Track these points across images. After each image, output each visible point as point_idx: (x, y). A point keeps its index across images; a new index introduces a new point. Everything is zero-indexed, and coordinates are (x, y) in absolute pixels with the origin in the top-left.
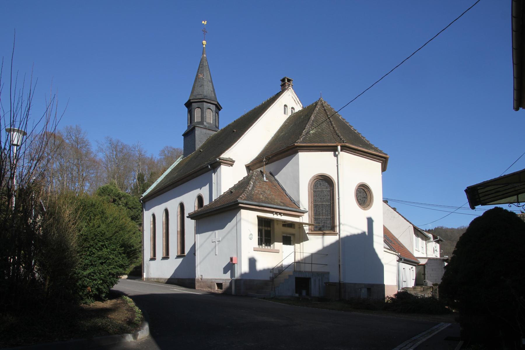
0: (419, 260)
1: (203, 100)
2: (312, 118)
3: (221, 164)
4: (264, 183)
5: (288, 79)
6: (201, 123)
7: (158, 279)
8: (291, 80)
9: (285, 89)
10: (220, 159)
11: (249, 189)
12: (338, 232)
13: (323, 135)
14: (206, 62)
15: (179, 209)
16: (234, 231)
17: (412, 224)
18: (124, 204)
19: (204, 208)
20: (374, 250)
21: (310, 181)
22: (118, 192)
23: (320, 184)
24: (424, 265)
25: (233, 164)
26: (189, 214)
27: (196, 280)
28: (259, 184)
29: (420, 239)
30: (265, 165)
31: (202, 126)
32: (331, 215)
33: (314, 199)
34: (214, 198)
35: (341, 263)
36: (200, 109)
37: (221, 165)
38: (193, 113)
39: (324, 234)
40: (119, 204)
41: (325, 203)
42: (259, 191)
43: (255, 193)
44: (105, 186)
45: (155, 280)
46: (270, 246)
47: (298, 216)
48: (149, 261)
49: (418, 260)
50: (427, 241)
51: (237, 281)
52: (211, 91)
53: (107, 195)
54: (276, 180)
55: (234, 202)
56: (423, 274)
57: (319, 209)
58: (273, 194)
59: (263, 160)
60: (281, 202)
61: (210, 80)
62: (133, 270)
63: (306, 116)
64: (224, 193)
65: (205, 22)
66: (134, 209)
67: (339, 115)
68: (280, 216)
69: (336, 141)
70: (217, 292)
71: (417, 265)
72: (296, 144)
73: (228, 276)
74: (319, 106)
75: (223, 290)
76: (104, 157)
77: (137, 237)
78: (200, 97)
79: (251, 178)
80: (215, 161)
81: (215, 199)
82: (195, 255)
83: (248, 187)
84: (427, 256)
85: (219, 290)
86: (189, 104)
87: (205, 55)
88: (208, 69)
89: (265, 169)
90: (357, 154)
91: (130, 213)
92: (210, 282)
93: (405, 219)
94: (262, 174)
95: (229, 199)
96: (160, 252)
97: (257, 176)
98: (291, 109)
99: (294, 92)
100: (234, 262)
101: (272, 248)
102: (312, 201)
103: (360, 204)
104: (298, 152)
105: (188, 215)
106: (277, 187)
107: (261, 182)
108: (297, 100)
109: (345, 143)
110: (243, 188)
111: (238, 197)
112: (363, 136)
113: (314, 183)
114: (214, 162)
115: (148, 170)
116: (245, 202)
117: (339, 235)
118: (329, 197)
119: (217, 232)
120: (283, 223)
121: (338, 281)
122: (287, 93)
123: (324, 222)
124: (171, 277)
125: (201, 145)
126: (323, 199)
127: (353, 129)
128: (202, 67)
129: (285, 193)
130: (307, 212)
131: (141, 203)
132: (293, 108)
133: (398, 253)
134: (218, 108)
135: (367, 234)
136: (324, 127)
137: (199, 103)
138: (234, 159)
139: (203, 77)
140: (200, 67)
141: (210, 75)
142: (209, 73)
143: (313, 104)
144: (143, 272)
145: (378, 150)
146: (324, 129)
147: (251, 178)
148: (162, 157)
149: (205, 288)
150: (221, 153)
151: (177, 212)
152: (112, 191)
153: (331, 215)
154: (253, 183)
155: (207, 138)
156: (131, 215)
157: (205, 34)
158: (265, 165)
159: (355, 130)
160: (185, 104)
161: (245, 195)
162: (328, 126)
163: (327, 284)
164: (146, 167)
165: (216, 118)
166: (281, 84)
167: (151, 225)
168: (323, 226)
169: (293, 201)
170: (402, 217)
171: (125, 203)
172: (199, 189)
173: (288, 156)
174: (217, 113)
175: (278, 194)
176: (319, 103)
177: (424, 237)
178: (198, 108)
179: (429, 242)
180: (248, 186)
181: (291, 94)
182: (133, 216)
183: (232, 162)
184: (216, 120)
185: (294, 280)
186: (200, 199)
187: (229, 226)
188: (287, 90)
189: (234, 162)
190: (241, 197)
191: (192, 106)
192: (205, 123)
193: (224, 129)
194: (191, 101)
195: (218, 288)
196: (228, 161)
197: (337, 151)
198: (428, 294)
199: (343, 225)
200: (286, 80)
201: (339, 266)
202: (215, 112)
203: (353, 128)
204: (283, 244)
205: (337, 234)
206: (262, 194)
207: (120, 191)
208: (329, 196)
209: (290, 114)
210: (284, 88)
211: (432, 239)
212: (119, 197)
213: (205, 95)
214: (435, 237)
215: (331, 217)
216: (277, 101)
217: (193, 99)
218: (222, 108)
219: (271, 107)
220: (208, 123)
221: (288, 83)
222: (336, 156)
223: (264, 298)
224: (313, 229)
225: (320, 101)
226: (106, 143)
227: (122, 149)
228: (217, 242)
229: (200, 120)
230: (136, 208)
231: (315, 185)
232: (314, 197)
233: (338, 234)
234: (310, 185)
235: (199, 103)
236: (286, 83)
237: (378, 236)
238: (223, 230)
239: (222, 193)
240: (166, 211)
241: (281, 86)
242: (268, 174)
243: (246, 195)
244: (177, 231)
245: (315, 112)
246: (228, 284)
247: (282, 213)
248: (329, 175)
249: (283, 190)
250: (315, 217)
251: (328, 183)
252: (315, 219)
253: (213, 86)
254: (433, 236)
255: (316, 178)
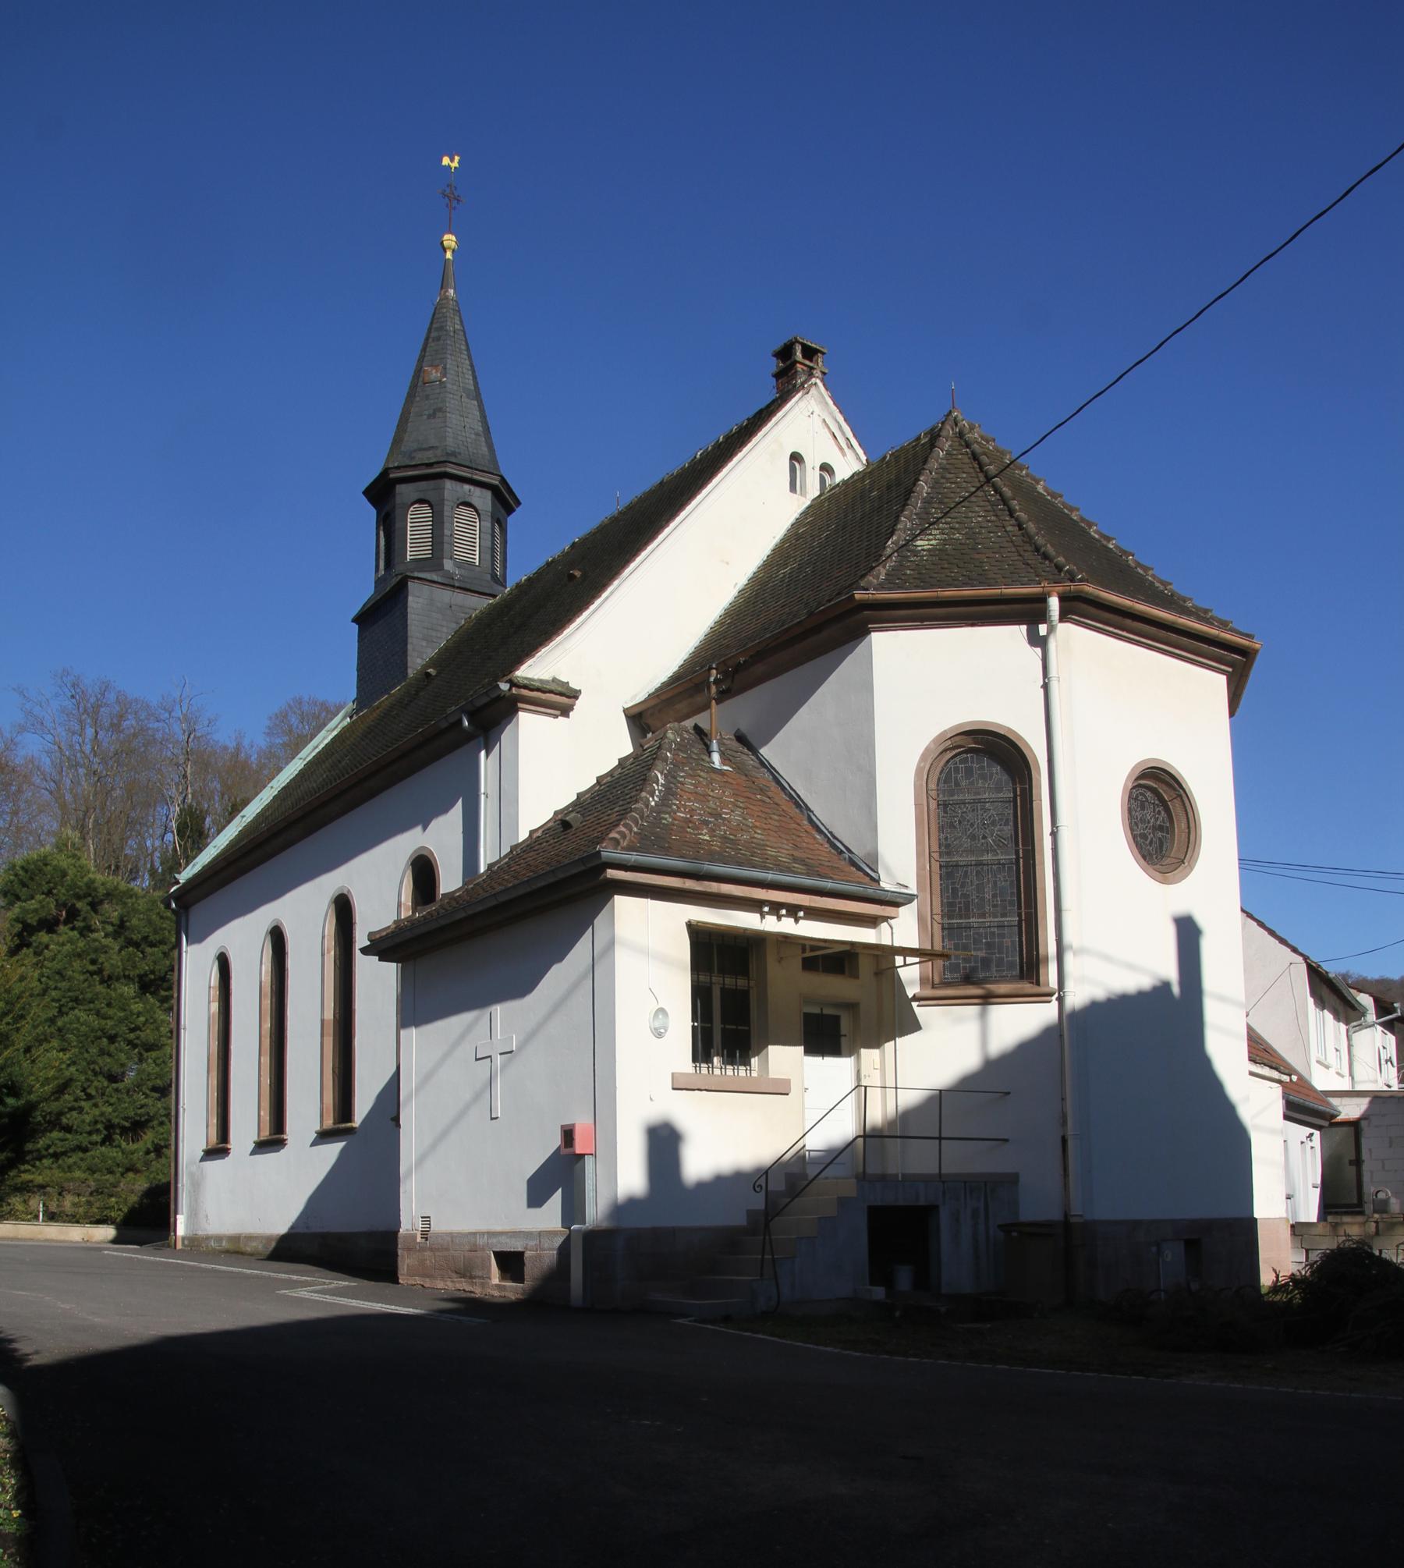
0: (1335, 1101)
1: (443, 469)
2: (924, 487)
3: (520, 705)
4: (714, 776)
5: (803, 345)
6: (434, 562)
7: (235, 1239)
8: (816, 352)
9: (795, 385)
10: (513, 684)
11: (647, 804)
12: (1056, 987)
13: (977, 556)
14: (457, 318)
15: (330, 923)
16: (583, 996)
17: (1301, 954)
18: (110, 928)
19: (442, 906)
20: (1206, 1063)
21: (923, 758)
22: (86, 879)
23: (969, 772)
24: (1355, 1125)
25: (571, 708)
26: (370, 934)
27: (400, 1241)
28: (691, 784)
29: (1328, 1016)
30: (718, 702)
31: (435, 577)
32: (1019, 907)
33: (943, 841)
34: (487, 856)
35: (1070, 1131)
36: (431, 505)
37: (516, 711)
38: (398, 525)
39: (987, 999)
40: (89, 929)
41: (990, 856)
42: (692, 811)
43: (674, 819)
44: (35, 857)
45: (224, 1243)
46: (746, 1062)
47: (872, 921)
48: (202, 1160)
49: (1329, 1104)
50: (1355, 1024)
51: (592, 1237)
52: (477, 434)
53: (43, 893)
54: (763, 764)
55: (582, 860)
56: (1351, 1163)
57: (963, 886)
58: (757, 824)
59: (709, 676)
60: (795, 859)
61: (473, 388)
62: (141, 1203)
63: (889, 488)
64: (532, 832)
65: (452, 160)
66: (152, 945)
67: (1034, 479)
68: (792, 920)
69: (1037, 576)
70: (496, 1293)
71: (1326, 1124)
72: (859, 595)
73: (550, 1217)
74: (949, 443)
75: (528, 1283)
76: (47, 752)
77: (164, 1062)
78: (429, 457)
79: (654, 759)
80: (494, 695)
81: (489, 862)
82: (398, 1125)
83: (644, 794)
84: (1353, 1086)
85: (509, 1284)
86: (381, 493)
87: (451, 292)
88: (463, 347)
89: (717, 718)
90: (1128, 631)
91: (134, 963)
92: (467, 1248)
93: (1272, 933)
94: (702, 739)
95: (558, 855)
96: (246, 1124)
97: (681, 747)
98: (817, 472)
99: (830, 402)
100: (578, 1151)
101: (754, 1074)
102: (935, 847)
103: (1144, 857)
104: (868, 632)
105: (369, 943)
106: (769, 793)
107: (702, 774)
108: (843, 433)
109: (1081, 580)
110: (621, 803)
111: (600, 840)
112: (1141, 562)
113: (939, 769)
114: (485, 700)
115: (223, 795)
116: (634, 857)
117: (1061, 1000)
118: (1011, 826)
119: (498, 1010)
120: (808, 954)
121: (1055, 1214)
122: (802, 404)
123: (987, 944)
124: (292, 1228)
125: (431, 652)
126: (984, 837)
127: (1097, 536)
128: (438, 339)
129: (806, 822)
130: (910, 901)
131: (173, 910)
132: (826, 468)
133: (1290, 1075)
134: (505, 500)
135: (1176, 989)
136: (978, 522)
137: (423, 485)
138: (573, 685)
139: (445, 376)
140: (430, 340)
141: (474, 372)
142: (467, 362)
143: (918, 438)
144: (176, 1213)
145: (1212, 617)
146: (979, 533)
147: (654, 759)
148: (279, 741)
149: (443, 1278)
150: (519, 661)
151: (323, 937)
152: (64, 874)
153: (1019, 907)
154: (666, 777)
155: (455, 627)
156: (137, 972)
157: (455, 208)
158: (718, 702)
159: (1109, 539)
160: (366, 493)
161: (631, 830)
162: (993, 518)
163: (1014, 1234)
164: (216, 785)
165: (493, 544)
166: (774, 370)
167: (209, 1002)
168: (986, 963)
169: (847, 855)
170: (1261, 924)
171: (116, 921)
172: (419, 829)
173: (821, 654)
174: (499, 522)
175: (777, 824)
176: (949, 431)
177: (1340, 1007)
178: (421, 501)
179: (1361, 1027)
180: (641, 790)
181: (817, 409)
182: (146, 975)
183: (568, 697)
184: (493, 549)
185: (861, 1222)
186: (423, 870)
187: (557, 978)
188: (800, 394)
189: (574, 695)
190: (615, 839)
191: (394, 496)
192: (448, 565)
193: (529, 579)
194: (391, 476)
195: (503, 1278)
196: (551, 692)
197: (1044, 622)
198: (1398, 1246)
199: (1074, 954)
200: (798, 349)
201: (1064, 1141)
202: (489, 519)
203: (1096, 532)
204: (808, 1052)
205: (1051, 995)
206: (706, 823)
207: (94, 873)
208: (1011, 823)
209: (813, 491)
210: (786, 385)
211: (1371, 1016)
212: (90, 899)
213: (450, 449)
214: (1383, 1008)
215: (1020, 921)
216: (760, 434)
217: (398, 468)
218: (518, 503)
219: (735, 460)
220: (461, 564)
221: (807, 362)
222: (1037, 641)
223: (727, 1319)
224: (937, 980)
225: (951, 422)
226: (57, 695)
227: (121, 717)
228: (499, 1060)
229: (426, 552)
230: (162, 942)
231: (944, 775)
232: (941, 829)
233: (1056, 995)
234: (924, 775)
235: (424, 483)
236: (796, 362)
237: (1222, 999)
238: (529, 999)
239: (523, 835)
240: (277, 938)
241: (774, 379)
242: (728, 742)
243: (635, 829)
244: (322, 1021)
245: (933, 464)
246: (549, 1255)
247: (799, 908)
248: (1010, 730)
249: (798, 805)
250: (946, 921)
251: (1002, 766)
252: (949, 931)
253: (483, 417)
254: (1377, 1001)
255: (949, 742)
